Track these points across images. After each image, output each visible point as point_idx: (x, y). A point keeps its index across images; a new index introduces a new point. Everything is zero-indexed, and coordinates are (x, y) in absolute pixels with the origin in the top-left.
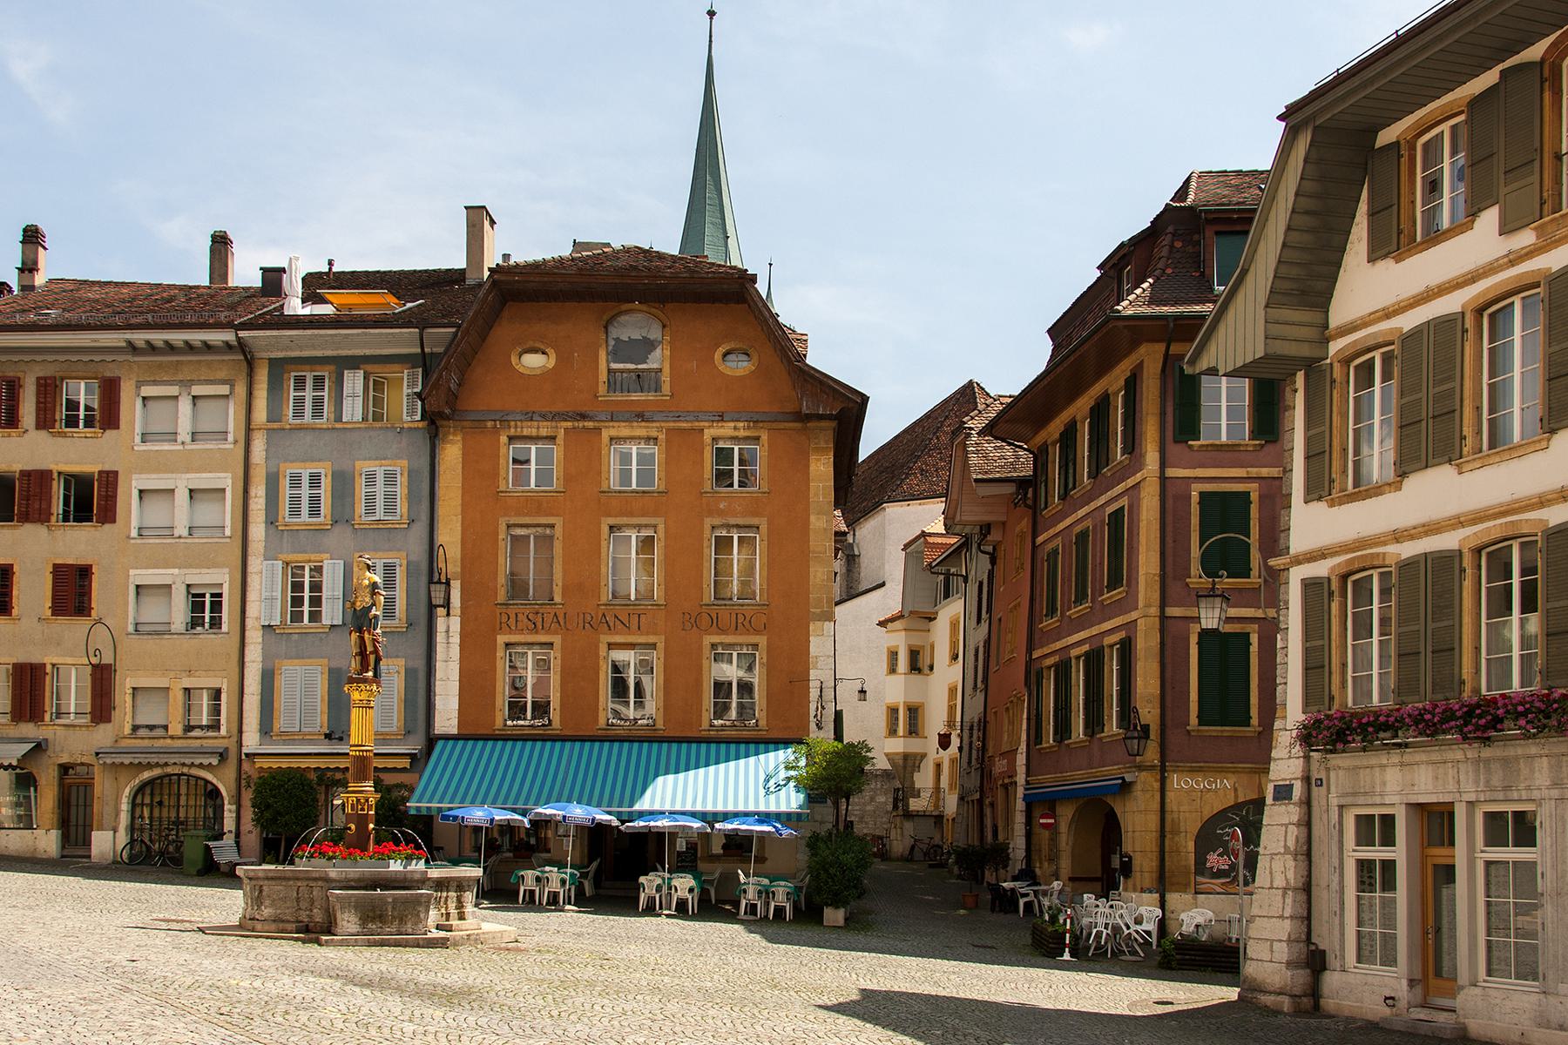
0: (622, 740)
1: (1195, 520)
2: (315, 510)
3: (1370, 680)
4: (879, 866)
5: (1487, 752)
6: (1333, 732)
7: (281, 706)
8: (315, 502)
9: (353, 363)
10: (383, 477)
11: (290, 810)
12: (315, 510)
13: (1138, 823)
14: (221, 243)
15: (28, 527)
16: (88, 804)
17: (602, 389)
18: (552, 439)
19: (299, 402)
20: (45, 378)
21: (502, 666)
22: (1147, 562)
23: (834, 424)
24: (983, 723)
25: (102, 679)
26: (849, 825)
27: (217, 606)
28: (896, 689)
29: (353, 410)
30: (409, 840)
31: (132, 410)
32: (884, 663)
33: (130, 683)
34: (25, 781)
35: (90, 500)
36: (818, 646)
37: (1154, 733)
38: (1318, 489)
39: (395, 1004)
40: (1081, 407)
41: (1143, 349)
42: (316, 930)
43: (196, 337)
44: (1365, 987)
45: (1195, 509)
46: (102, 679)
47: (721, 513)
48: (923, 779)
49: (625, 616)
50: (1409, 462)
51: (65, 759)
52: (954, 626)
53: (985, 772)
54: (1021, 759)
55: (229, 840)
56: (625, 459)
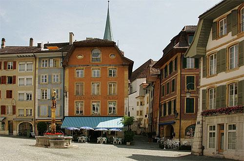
0: (94, 117)
1: (186, 81)
2: (46, 81)
3: (212, 105)
4: (135, 135)
5: (230, 115)
6: (206, 113)
7: (41, 112)
8: (46, 80)
9: (52, 58)
10: (56, 75)
11: (43, 128)
12: (46, 81)
13: (176, 128)
14: (31, 39)
15: (3, 85)
16: (12, 127)
17: (91, 61)
18: (83, 69)
19: (43, 64)
20: (240, 112)
21: (75, 105)
22: (178, 87)
23: (128, 66)
24: (152, 113)
25: (14, 107)
26: (131, 129)
27: (31, 96)
28: (138, 108)
29: (52, 65)
30: (61, 132)
31: (18, 66)
32: (137, 104)
33: (18, 108)
34: (3, 123)
35: (12, 80)
36: (126, 102)
37: (179, 114)
38: (204, 76)
39: (60, 157)
40: (169, 62)
41: (178, 54)
42: (47, 146)
43: (28, 54)
44: (210, 151)
45: (186, 79)
46: (14, 107)
47: (110, 81)
48: (143, 122)
49: (95, 97)
50: (218, 71)
51: (9, 120)
52: (148, 98)
53: (152, 121)
54: (158, 119)
55: (34, 132)
56: (95, 72)
